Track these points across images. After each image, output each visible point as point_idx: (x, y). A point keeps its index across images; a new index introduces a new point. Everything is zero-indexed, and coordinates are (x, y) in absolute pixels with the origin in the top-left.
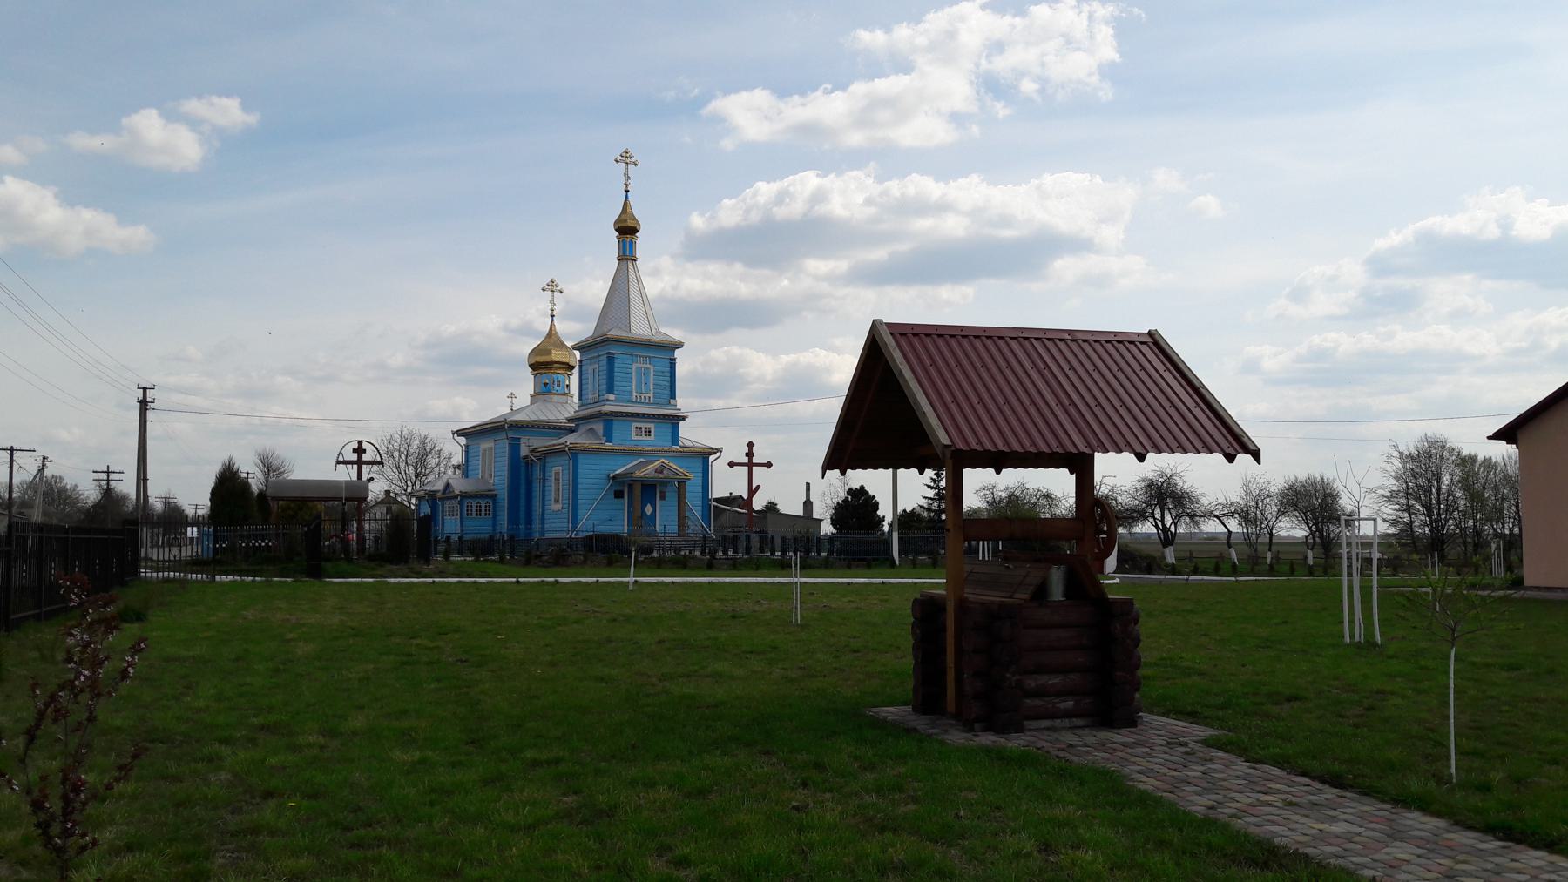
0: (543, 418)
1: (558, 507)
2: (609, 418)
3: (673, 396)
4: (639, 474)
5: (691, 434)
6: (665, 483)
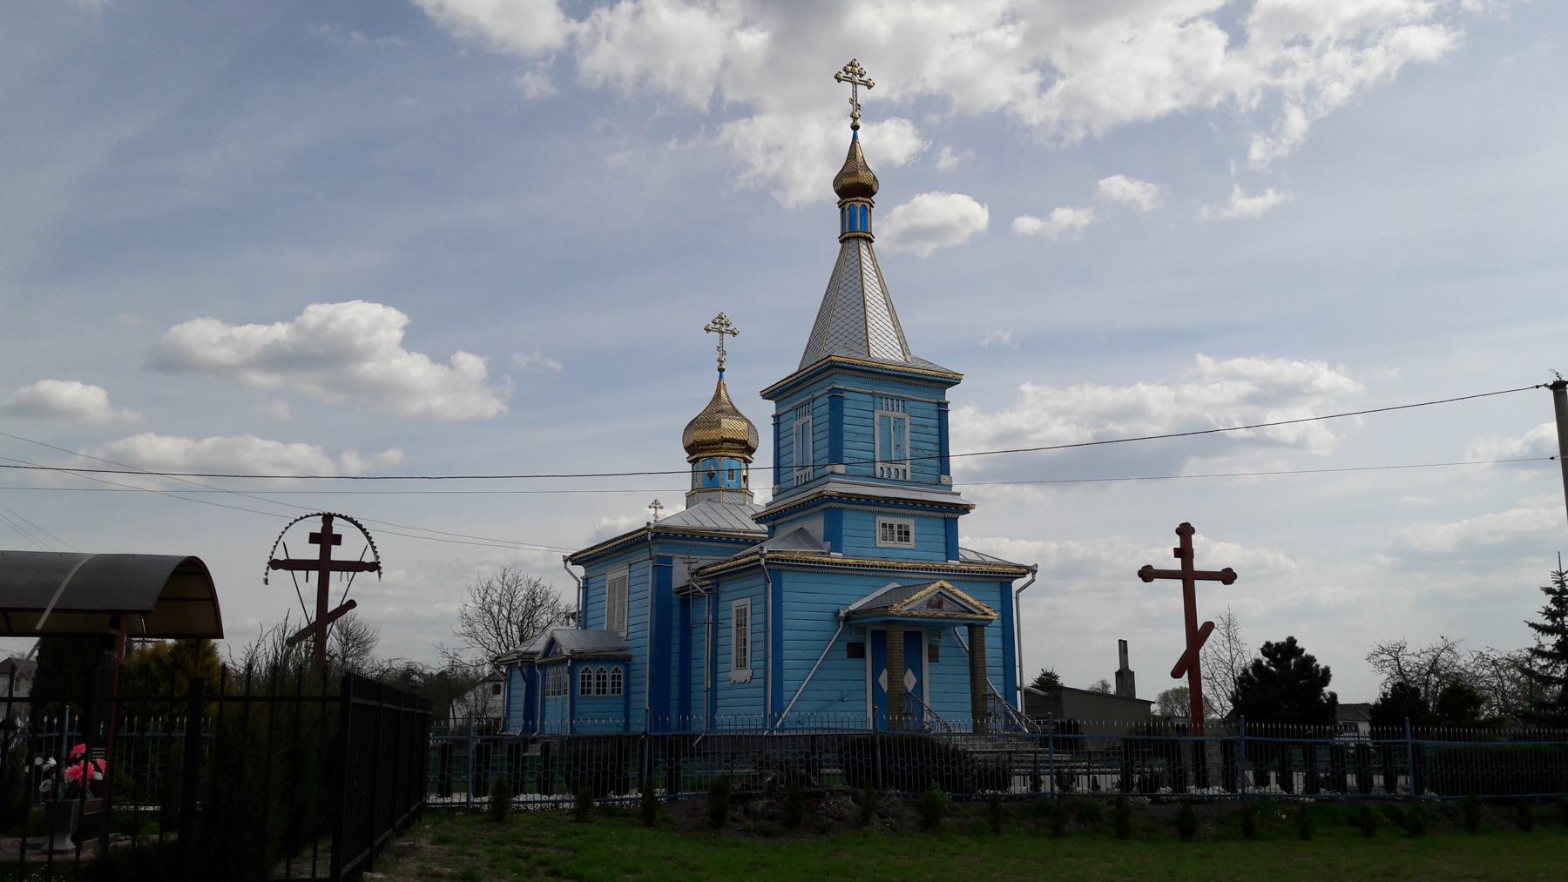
0: (709, 525)
1: (742, 675)
2: (834, 508)
3: (944, 468)
4: (900, 608)
5: (978, 539)
6: (938, 628)
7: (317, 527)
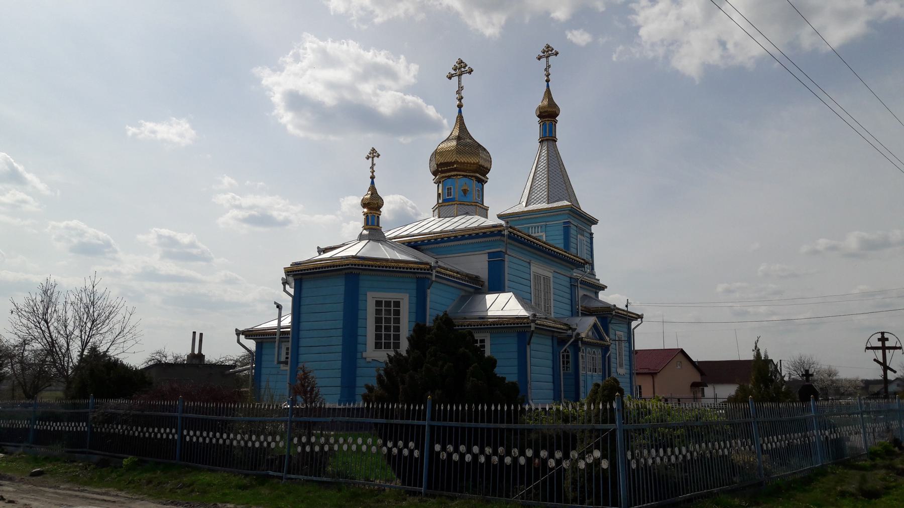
7: (880, 336)
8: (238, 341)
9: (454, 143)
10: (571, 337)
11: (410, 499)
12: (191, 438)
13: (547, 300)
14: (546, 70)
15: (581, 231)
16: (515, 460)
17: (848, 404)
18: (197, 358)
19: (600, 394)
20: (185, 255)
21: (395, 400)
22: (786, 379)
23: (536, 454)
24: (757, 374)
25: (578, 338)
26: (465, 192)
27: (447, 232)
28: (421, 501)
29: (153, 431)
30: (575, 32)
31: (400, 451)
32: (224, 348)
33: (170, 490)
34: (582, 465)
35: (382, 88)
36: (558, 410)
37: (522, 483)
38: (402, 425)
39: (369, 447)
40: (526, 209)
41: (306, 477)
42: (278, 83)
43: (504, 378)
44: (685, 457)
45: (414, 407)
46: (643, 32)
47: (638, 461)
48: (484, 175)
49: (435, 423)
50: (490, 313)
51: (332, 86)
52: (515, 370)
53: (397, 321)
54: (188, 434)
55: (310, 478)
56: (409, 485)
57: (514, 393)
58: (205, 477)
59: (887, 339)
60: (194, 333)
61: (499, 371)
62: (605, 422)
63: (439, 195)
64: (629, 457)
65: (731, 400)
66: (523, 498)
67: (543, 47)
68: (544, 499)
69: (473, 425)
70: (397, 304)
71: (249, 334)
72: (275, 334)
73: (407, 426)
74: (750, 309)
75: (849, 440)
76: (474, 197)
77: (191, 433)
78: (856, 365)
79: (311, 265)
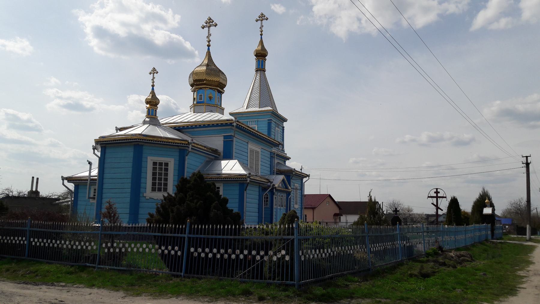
7: (435, 190)
8: (63, 184)
9: (205, 68)
10: (270, 186)
11: (175, 279)
12: (36, 243)
13: (257, 165)
14: (260, 28)
15: (278, 125)
16: (237, 256)
17: (417, 227)
18: (34, 194)
19: (286, 219)
20: (24, 127)
21: (167, 222)
22: (385, 212)
23: (250, 253)
24: (369, 210)
25: (274, 187)
26: (210, 98)
27: (198, 122)
28: (181, 280)
29: (10, 239)
30: (276, 5)
31: (169, 252)
32: (52, 187)
33: (22, 275)
34: (275, 258)
35: (157, 28)
36: (263, 229)
37: (241, 269)
38: (171, 237)
39: (150, 250)
40: (246, 111)
41: (110, 267)
42: (89, 21)
43: (233, 210)
44: (330, 254)
45: (179, 226)
46: (315, 9)
47: (305, 256)
48: (222, 89)
49: (191, 236)
50: (223, 172)
51: (124, 24)
52: (237, 205)
53: (166, 174)
54: (34, 241)
55: (112, 267)
56: (174, 271)
57: (238, 219)
58: (46, 267)
59: (439, 192)
60: (33, 178)
61: (229, 206)
62: (288, 235)
63: (194, 99)
64: (301, 254)
65: (355, 223)
66: (241, 278)
67: (259, 14)
68: (253, 278)
69: (214, 236)
70: (167, 164)
71: (70, 179)
72: (87, 180)
73: (174, 237)
74: (367, 173)
75: (416, 247)
76: (216, 101)
77: (36, 240)
78: (422, 206)
79: (112, 138)
